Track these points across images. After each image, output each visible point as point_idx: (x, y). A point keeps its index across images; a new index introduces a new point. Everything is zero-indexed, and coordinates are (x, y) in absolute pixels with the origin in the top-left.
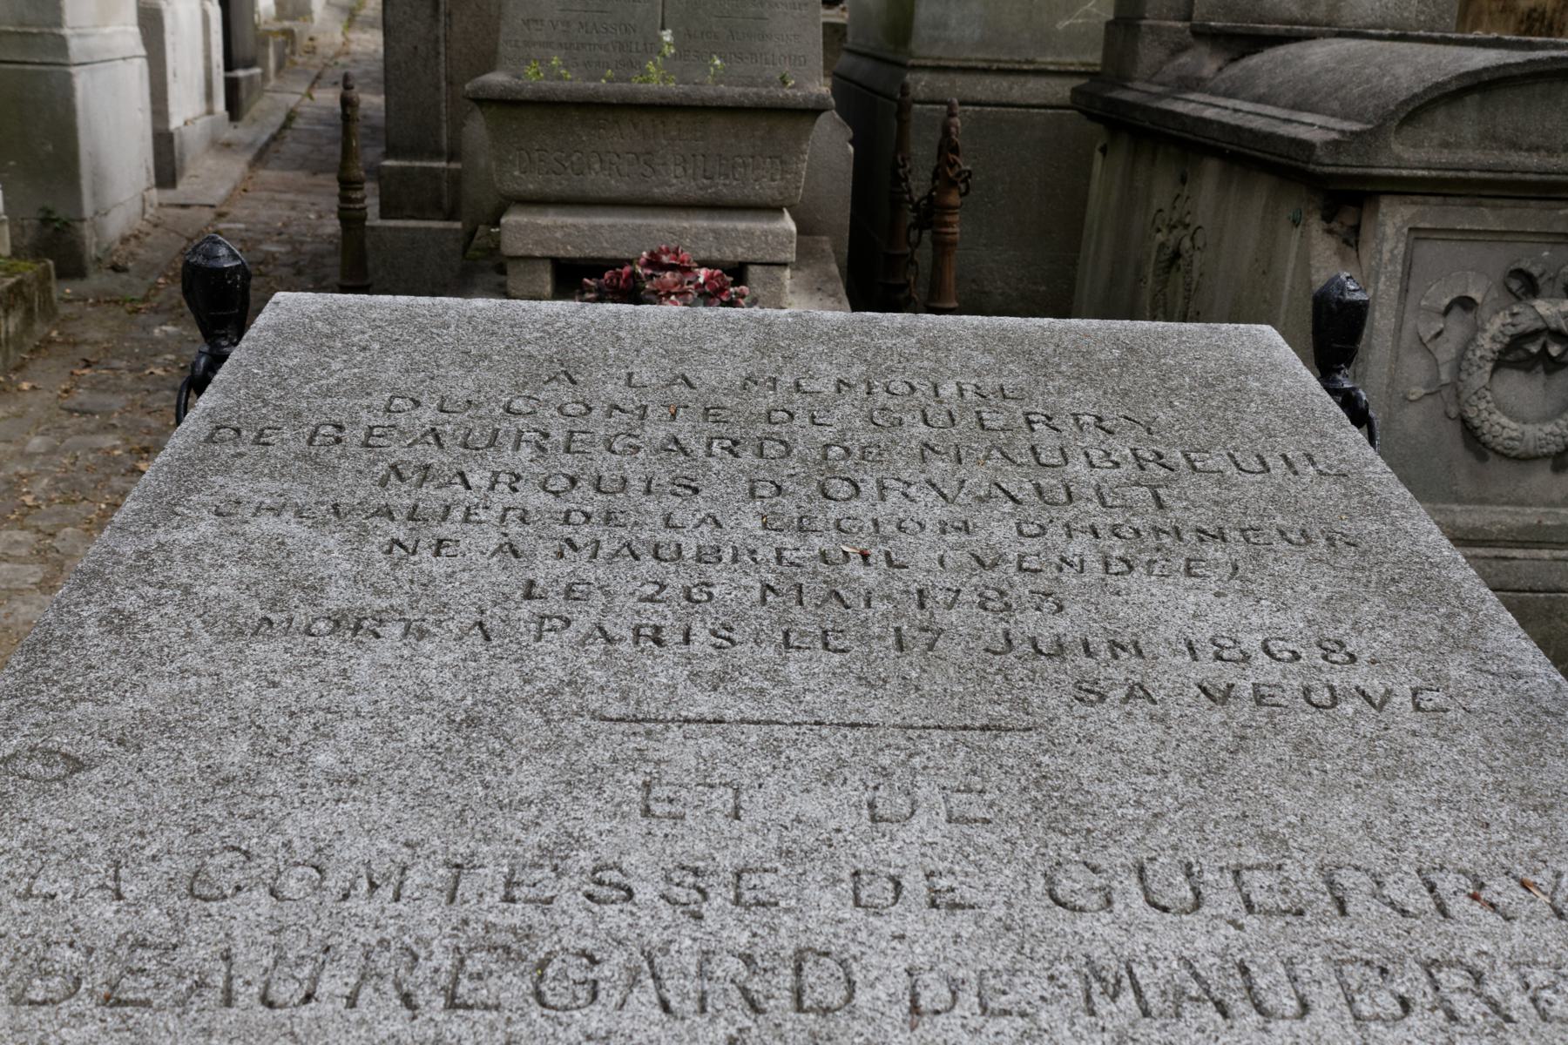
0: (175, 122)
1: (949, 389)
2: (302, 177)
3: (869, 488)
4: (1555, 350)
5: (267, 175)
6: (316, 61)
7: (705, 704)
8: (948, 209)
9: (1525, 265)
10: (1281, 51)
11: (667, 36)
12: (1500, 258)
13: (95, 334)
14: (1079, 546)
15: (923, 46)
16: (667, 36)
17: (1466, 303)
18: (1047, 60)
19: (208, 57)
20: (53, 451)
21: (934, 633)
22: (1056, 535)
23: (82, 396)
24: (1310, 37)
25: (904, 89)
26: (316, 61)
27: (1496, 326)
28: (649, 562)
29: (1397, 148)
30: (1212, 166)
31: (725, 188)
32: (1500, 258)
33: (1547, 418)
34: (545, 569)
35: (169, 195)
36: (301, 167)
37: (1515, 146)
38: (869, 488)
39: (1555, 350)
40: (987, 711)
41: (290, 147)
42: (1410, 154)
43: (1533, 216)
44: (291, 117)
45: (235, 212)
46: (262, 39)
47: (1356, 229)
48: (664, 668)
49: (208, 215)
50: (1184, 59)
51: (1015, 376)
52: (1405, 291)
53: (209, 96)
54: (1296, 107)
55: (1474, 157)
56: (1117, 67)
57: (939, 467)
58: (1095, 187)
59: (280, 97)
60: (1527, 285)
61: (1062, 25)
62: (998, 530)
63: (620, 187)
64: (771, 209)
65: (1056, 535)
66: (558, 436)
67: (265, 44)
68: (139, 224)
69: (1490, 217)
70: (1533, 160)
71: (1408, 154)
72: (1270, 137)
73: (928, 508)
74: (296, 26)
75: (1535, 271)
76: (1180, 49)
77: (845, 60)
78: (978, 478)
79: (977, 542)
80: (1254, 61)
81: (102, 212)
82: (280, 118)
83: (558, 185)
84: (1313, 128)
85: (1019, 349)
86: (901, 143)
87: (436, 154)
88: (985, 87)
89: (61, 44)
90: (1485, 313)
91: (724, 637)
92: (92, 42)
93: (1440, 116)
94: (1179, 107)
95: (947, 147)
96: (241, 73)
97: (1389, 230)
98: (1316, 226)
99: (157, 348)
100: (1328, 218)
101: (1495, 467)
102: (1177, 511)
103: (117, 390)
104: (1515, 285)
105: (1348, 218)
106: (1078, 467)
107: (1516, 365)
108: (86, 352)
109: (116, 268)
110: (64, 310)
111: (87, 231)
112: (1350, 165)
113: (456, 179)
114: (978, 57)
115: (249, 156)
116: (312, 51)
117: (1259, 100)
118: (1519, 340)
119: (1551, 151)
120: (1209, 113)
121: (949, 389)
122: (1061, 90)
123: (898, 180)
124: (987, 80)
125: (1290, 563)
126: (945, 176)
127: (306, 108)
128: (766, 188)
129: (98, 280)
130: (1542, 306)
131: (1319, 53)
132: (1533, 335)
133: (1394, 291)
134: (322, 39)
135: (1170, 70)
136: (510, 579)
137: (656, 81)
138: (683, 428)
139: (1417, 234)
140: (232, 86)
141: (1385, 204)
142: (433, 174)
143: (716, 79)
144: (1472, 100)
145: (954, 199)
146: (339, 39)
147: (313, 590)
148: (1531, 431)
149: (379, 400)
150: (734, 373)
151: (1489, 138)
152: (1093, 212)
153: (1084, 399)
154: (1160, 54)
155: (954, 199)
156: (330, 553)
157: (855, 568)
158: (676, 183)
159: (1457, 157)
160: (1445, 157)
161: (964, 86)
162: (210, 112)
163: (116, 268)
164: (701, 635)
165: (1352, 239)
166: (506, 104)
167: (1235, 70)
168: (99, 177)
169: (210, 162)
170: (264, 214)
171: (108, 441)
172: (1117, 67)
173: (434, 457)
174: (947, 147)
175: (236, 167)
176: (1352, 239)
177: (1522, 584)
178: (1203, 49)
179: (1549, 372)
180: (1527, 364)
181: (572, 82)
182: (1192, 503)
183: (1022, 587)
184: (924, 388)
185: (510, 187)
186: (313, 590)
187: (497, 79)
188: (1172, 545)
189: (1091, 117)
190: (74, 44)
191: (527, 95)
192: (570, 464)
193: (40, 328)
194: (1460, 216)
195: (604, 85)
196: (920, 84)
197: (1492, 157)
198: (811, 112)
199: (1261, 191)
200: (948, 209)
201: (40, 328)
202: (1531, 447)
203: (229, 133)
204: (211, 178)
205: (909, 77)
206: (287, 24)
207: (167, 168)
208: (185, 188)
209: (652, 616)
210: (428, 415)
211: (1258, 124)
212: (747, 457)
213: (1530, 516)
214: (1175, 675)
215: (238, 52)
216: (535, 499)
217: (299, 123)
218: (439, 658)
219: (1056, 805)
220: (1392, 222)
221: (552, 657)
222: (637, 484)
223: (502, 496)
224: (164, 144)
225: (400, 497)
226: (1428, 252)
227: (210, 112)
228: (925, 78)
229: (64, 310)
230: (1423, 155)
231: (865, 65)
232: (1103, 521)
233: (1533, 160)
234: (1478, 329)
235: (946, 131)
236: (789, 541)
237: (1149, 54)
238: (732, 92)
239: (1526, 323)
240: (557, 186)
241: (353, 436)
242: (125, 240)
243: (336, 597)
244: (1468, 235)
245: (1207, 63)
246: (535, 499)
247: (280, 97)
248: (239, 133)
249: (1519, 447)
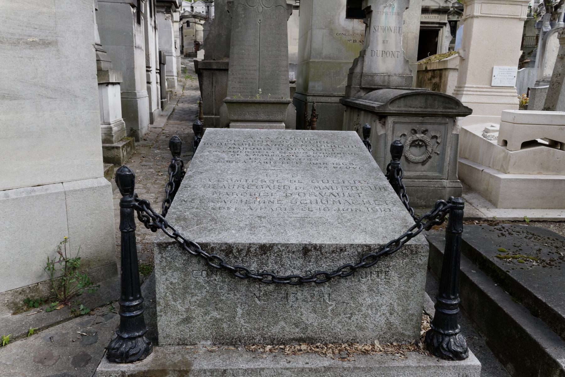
0: (153, 111)
1: (306, 139)
2: (178, 122)
3: (294, 149)
4: (420, 143)
5: (171, 121)
6: (177, 97)
7: (273, 168)
8: (314, 121)
9: (414, 128)
10: (375, 91)
11: (260, 90)
12: (410, 127)
13: (143, 152)
14: (322, 155)
15: (310, 91)
16: (260, 90)
17: (404, 135)
18: (336, 94)
19: (158, 97)
20: (141, 172)
21: (301, 162)
22: (318, 154)
23: (144, 163)
24: (381, 89)
25: (306, 100)
26: (177, 97)
27: (410, 139)
28: (265, 156)
29: (390, 107)
30: (363, 112)
31: (272, 118)
32: (410, 127)
33: (420, 156)
34: (252, 157)
35: (152, 126)
36: (178, 120)
37: (410, 107)
38: (294, 149)
39: (420, 143)
40: (306, 169)
41: (175, 116)
42: (392, 109)
43: (415, 119)
44: (174, 110)
45: (166, 129)
46: (167, 93)
47: (385, 122)
48: (268, 165)
49: (161, 130)
50: (359, 93)
51: (316, 137)
52: (393, 133)
53: (158, 105)
54: (375, 101)
55: (403, 109)
56: (347, 95)
57: (303, 147)
58: (344, 118)
59: (171, 106)
60: (415, 132)
61: (338, 87)
62: (311, 153)
63: (252, 118)
64: (280, 122)
65: (318, 154)
66: (251, 144)
67: (167, 94)
68: (147, 131)
69: (407, 120)
70: (414, 109)
71: (392, 109)
72: (369, 106)
73: (302, 151)
74: (173, 90)
75: (416, 129)
76: (359, 91)
77: (295, 95)
78: (309, 148)
79: (308, 154)
80: (370, 93)
81: (142, 129)
82: (172, 110)
83: (240, 118)
84: (376, 104)
85: (317, 134)
86: (306, 110)
87: (213, 114)
88: (319, 99)
89: (135, 94)
90: (408, 137)
91: (275, 163)
92: (140, 93)
93: (397, 102)
94: (357, 102)
95: (314, 110)
96: (163, 100)
97: (390, 122)
98: (378, 122)
99: (157, 154)
100: (380, 120)
101: (411, 165)
102: (335, 151)
103: (151, 162)
104: (413, 132)
105: (383, 121)
106: (323, 147)
107: (414, 146)
108: (143, 155)
109: (145, 140)
110: (136, 148)
111: (139, 132)
112: (381, 110)
113: (217, 119)
114: (321, 93)
115: (167, 118)
116: (176, 95)
117: (370, 100)
118: (414, 141)
119: (417, 108)
120: (361, 103)
121: (306, 139)
122: (337, 100)
123: (305, 117)
124: (324, 98)
125: (349, 156)
126: (314, 115)
127: (177, 107)
128: (279, 118)
129: (141, 142)
130: (418, 135)
131: (381, 91)
132: (416, 141)
133: (391, 133)
134: (178, 93)
135: (357, 95)
136: (248, 158)
137: (258, 98)
138: (268, 143)
139: (395, 123)
140: (162, 103)
141: (389, 117)
142: (212, 118)
143: (269, 98)
144: (402, 99)
145: (315, 119)
146: (182, 92)
147: (224, 159)
148: (417, 158)
149: (226, 140)
150: (275, 137)
151: (406, 106)
152: (344, 123)
153: (326, 140)
154: (355, 92)
155: (315, 119)
156: (224, 155)
157: (292, 157)
158: (262, 117)
159: (400, 109)
160: (398, 109)
161: (319, 99)
162: (158, 108)
163: (145, 140)
164: (272, 163)
165: (384, 124)
166: (230, 103)
167: (367, 95)
168: (141, 121)
169: (159, 119)
170: (172, 129)
171: (152, 170)
172: (347, 95)
173: (235, 146)
174: (314, 110)
175: (165, 120)
176: (384, 124)
177: (417, 185)
178: (362, 91)
179: (420, 147)
180: (416, 146)
181: (242, 99)
182: (337, 150)
183: (313, 158)
184: (302, 139)
185: (231, 118)
186: (224, 159)
187: (228, 98)
188: (334, 154)
189: (343, 105)
190: (138, 94)
191: (235, 101)
192: (254, 147)
193: (133, 151)
194: (402, 119)
195: (249, 99)
196: (310, 99)
197: (406, 109)
198: (287, 103)
199: (370, 115)
200: (314, 121)
201: (133, 151)
202: (417, 161)
203: (162, 113)
204: (160, 122)
205: (308, 97)
206: (170, 89)
207: (152, 122)
208: (155, 124)
209: (266, 161)
210: (233, 142)
211: (368, 104)
212: (277, 146)
213: (418, 173)
214: (330, 166)
215: (163, 96)
216: (249, 150)
217: (176, 111)
218: (240, 164)
219: (313, 175)
220: (390, 121)
221: (254, 164)
222: (263, 149)
223: (245, 150)
224: (151, 114)
225: (232, 150)
226: (397, 126)
227: (158, 108)
228: (311, 98)
229: (136, 148)
230: (394, 109)
231: (299, 95)
232: (325, 152)
233: (414, 109)
234: (407, 139)
235: (313, 107)
236: (283, 154)
237: (353, 92)
238: (273, 100)
239: (415, 138)
240: (240, 118)
241: (223, 144)
242: (145, 134)
243: (226, 159)
244: (404, 123)
245: (362, 94)
246: (249, 150)
247: (171, 106)
248: (164, 113)
249: (415, 161)
